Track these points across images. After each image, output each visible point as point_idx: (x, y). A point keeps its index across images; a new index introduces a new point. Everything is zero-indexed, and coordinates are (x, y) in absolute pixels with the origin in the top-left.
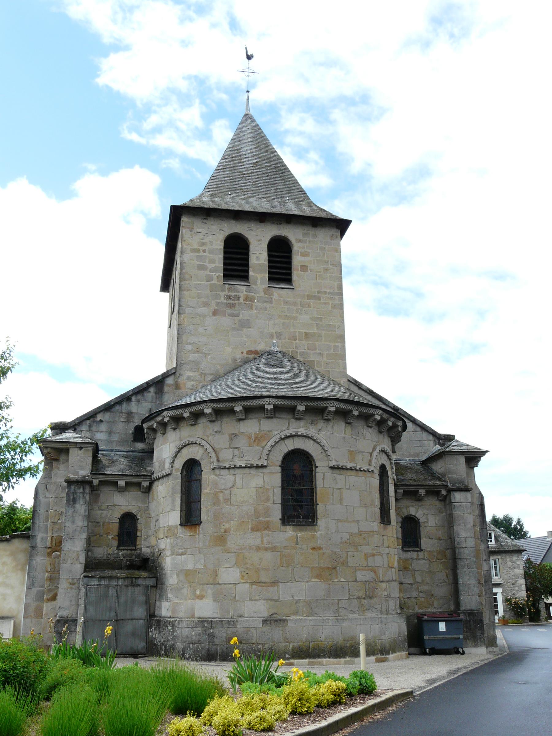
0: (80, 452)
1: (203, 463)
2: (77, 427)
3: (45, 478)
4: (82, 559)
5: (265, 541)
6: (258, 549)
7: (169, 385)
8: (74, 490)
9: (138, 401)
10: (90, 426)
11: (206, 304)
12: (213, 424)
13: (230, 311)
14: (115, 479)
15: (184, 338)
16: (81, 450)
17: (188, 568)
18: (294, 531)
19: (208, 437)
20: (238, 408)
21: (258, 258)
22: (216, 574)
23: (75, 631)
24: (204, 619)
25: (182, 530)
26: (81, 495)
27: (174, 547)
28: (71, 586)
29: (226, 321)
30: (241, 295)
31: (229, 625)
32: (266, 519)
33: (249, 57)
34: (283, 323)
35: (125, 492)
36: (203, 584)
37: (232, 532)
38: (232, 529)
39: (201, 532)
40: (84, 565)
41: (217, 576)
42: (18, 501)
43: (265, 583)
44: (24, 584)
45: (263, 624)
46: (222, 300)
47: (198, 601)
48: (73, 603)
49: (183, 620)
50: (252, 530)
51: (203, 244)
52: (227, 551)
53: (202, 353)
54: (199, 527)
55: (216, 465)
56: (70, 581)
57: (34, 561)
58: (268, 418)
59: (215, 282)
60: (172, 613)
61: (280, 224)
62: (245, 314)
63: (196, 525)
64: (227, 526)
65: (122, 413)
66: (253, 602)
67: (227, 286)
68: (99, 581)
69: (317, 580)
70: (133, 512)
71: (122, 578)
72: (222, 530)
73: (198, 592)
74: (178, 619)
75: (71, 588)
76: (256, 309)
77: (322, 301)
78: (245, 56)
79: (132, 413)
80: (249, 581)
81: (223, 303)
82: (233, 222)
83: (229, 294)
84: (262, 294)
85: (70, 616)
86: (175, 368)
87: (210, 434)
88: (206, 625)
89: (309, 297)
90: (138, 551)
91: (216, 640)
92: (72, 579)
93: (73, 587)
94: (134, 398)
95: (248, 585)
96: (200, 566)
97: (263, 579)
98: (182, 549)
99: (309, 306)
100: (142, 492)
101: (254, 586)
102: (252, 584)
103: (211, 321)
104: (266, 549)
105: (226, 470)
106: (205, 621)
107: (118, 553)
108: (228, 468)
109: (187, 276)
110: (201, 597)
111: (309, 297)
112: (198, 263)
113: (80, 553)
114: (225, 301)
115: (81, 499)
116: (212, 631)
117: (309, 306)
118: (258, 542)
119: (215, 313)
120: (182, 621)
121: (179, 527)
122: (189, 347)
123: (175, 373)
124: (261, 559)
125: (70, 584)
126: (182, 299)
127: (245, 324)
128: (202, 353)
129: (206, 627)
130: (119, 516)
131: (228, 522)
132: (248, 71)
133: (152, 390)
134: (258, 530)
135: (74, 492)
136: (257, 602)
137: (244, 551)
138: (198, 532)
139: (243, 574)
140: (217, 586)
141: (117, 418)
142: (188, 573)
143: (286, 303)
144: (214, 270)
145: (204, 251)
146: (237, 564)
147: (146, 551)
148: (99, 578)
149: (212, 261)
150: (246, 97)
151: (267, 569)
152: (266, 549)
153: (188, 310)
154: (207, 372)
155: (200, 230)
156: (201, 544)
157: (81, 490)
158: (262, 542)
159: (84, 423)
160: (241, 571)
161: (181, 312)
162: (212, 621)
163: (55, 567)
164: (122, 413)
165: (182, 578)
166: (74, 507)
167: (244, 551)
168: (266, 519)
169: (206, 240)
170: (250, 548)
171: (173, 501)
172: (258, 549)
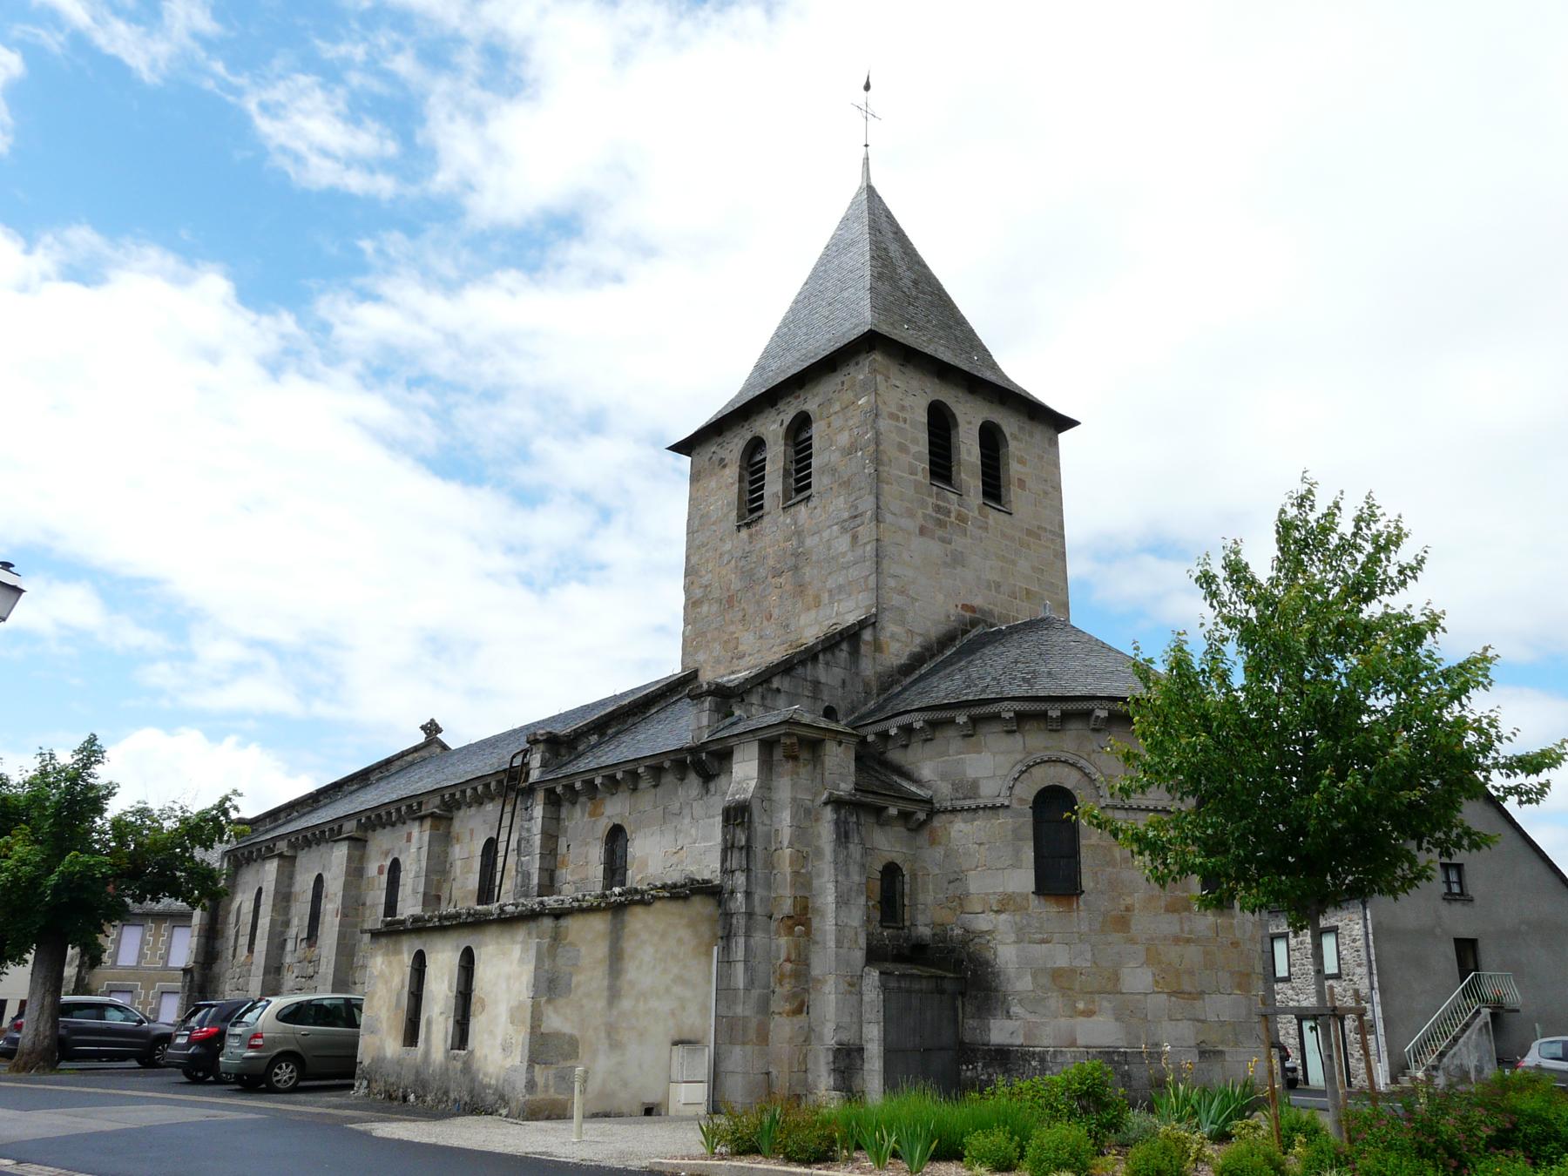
0: (840, 750)
1: (1079, 795)
2: (745, 696)
3: (761, 787)
4: (862, 942)
5: (1186, 928)
6: (1177, 940)
7: (867, 643)
8: (846, 818)
9: (827, 664)
10: (763, 698)
11: (911, 514)
12: (1096, 735)
13: (939, 532)
14: (880, 802)
15: (885, 564)
16: (840, 746)
17: (1057, 965)
18: (1214, 916)
19: (1089, 755)
20: (1055, 713)
21: (969, 453)
22: (1116, 977)
23: (862, 1069)
24: (1111, 1049)
25: (1039, 902)
26: (855, 826)
27: (1021, 929)
28: (850, 988)
29: (935, 548)
30: (953, 509)
31: (1151, 1058)
32: (1185, 895)
33: (867, 87)
34: (1002, 567)
35: (887, 828)
36: (1091, 993)
37: (1136, 911)
38: (1137, 905)
39: (1082, 907)
40: (865, 952)
41: (1118, 980)
42: (240, 795)
43: (1190, 994)
44: (709, 981)
45: (1200, 1057)
46: (930, 511)
47: (1081, 1019)
48: (855, 1019)
49: (1063, 1049)
50: (1167, 910)
51: (903, 408)
52: (1132, 941)
53: (908, 596)
54: (1078, 899)
55: (1109, 801)
56: (848, 978)
57: (752, 941)
58: (1051, 730)
59: (920, 477)
60: (1025, 1039)
61: (992, 403)
62: (959, 542)
63: (1073, 895)
64: (1129, 901)
65: (806, 681)
66: (1173, 1023)
67: (935, 488)
68: (899, 981)
69: (1239, 992)
70: (898, 862)
71: (925, 977)
72: (1123, 908)
73: (1081, 1006)
74: (1052, 1049)
75: (850, 992)
76: (971, 538)
77: (1042, 542)
78: (864, 83)
79: (820, 683)
80: (1166, 990)
81: (931, 517)
82: (936, 380)
83: (939, 503)
84: (976, 514)
85: (851, 1042)
86: (876, 615)
87: (1094, 751)
88: (1116, 1059)
89: (1029, 533)
90: (906, 931)
91: (1133, 1082)
92: (852, 976)
93: (853, 989)
94: (821, 657)
95: (1165, 996)
96: (1083, 963)
97: (1187, 988)
98: (1040, 933)
99: (1028, 547)
100: (909, 830)
101: (1173, 999)
102: (1170, 994)
103: (917, 543)
104: (1188, 941)
105: (1123, 812)
106: (1114, 1052)
107: (881, 933)
108: (1126, 809)
109: (885, 458)
110: (1089, 1013)
111: (1029, 533)
112: (898, 439)
113: (859, 930)
114: (934, 514)
115: (856, 834)
116: (1126, 1067)
117: (1028, 547)
118: (1176, 929)
119: (923, 531)
120: (1061, 1051)
121: (1032, 897)
122: (892, 583)
123: (874, 623)
124: (1182, 957)
125: (850, 985)
126: (881, 497)
127: (957, 560)
128: (908, 596)
129: (1118, 1062)
130: (881, 868)
131: (1131, 894)
132: (867, 113)
133: (845, 646)
134: (1175, 911)
135: (846, 822)
136: (1180, 1023)
137: (1156, 942)
138: (1075, 907)
139: (1157, 978)
140: (1118, 996)
141: (800, 690)
142: (1060, 979)
143: (1004, 535)
144: (917, 457)
145: (905, 421)
146: (1148, 962)
147: (924, 931)
148: (899, 976)
149: (915, 441)
150: (863, 155)
151: (1191, 973)
152: (1188, 941)
153: (889, 518)
154: (916, 631)
155: (898, 383)
156: (1084, 928)
157: (854, 819)
158: (1182, 929)
159: (754, 690)
160: (1154, 975)
161: (880, 519)
162: (1126, 1053)
163: (800, 955)
164: (806, 681)
165: (1044, 980)
166: (847, 848)
167: (1156, 942)
168: (1185, 895)
169: (906, 403)
170: (1165, 938)
171: (1017, 852)
172: (1177, 940)
